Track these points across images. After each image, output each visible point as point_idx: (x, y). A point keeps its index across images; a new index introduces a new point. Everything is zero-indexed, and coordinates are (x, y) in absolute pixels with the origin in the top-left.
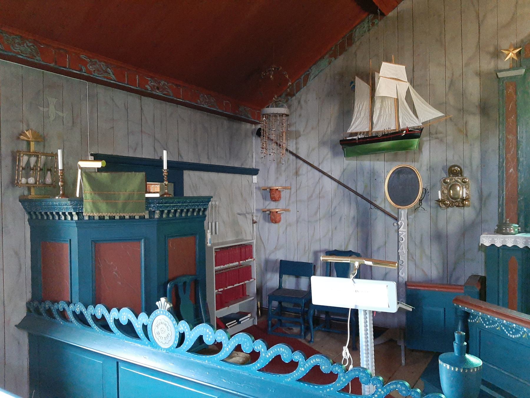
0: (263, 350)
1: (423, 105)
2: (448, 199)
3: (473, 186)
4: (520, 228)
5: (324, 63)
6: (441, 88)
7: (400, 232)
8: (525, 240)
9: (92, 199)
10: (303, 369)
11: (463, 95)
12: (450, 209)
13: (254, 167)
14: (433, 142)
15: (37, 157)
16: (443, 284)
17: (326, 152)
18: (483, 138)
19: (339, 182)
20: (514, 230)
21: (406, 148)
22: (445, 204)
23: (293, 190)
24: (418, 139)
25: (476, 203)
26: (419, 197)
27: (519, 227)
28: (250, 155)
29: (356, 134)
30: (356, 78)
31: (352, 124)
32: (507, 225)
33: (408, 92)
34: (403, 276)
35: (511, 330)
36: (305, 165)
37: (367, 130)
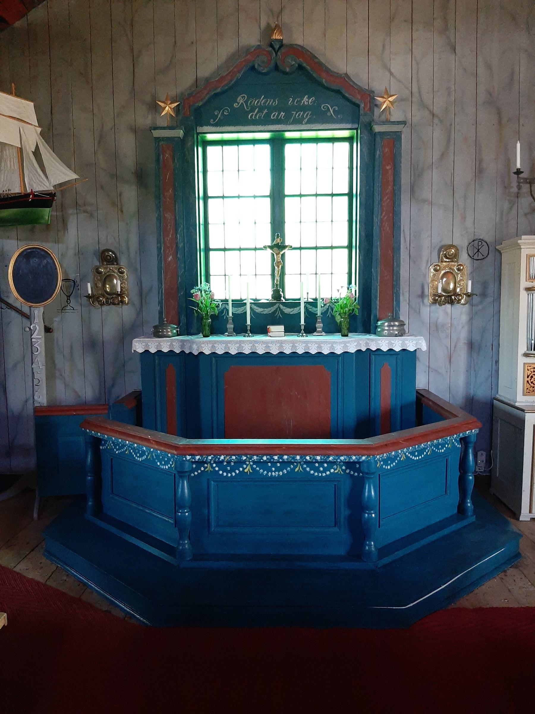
1: (54, 161)
4: (179, 330)
7: (33, 340)
8: (180, 344)
12: (105, 308)
14: (82, 216)
16: (100, 405)
20: (171, 331)
24: (49, 209)
25: (136, 301)
27: (177, 328)
34: (40, 400)
35: (139, 452)
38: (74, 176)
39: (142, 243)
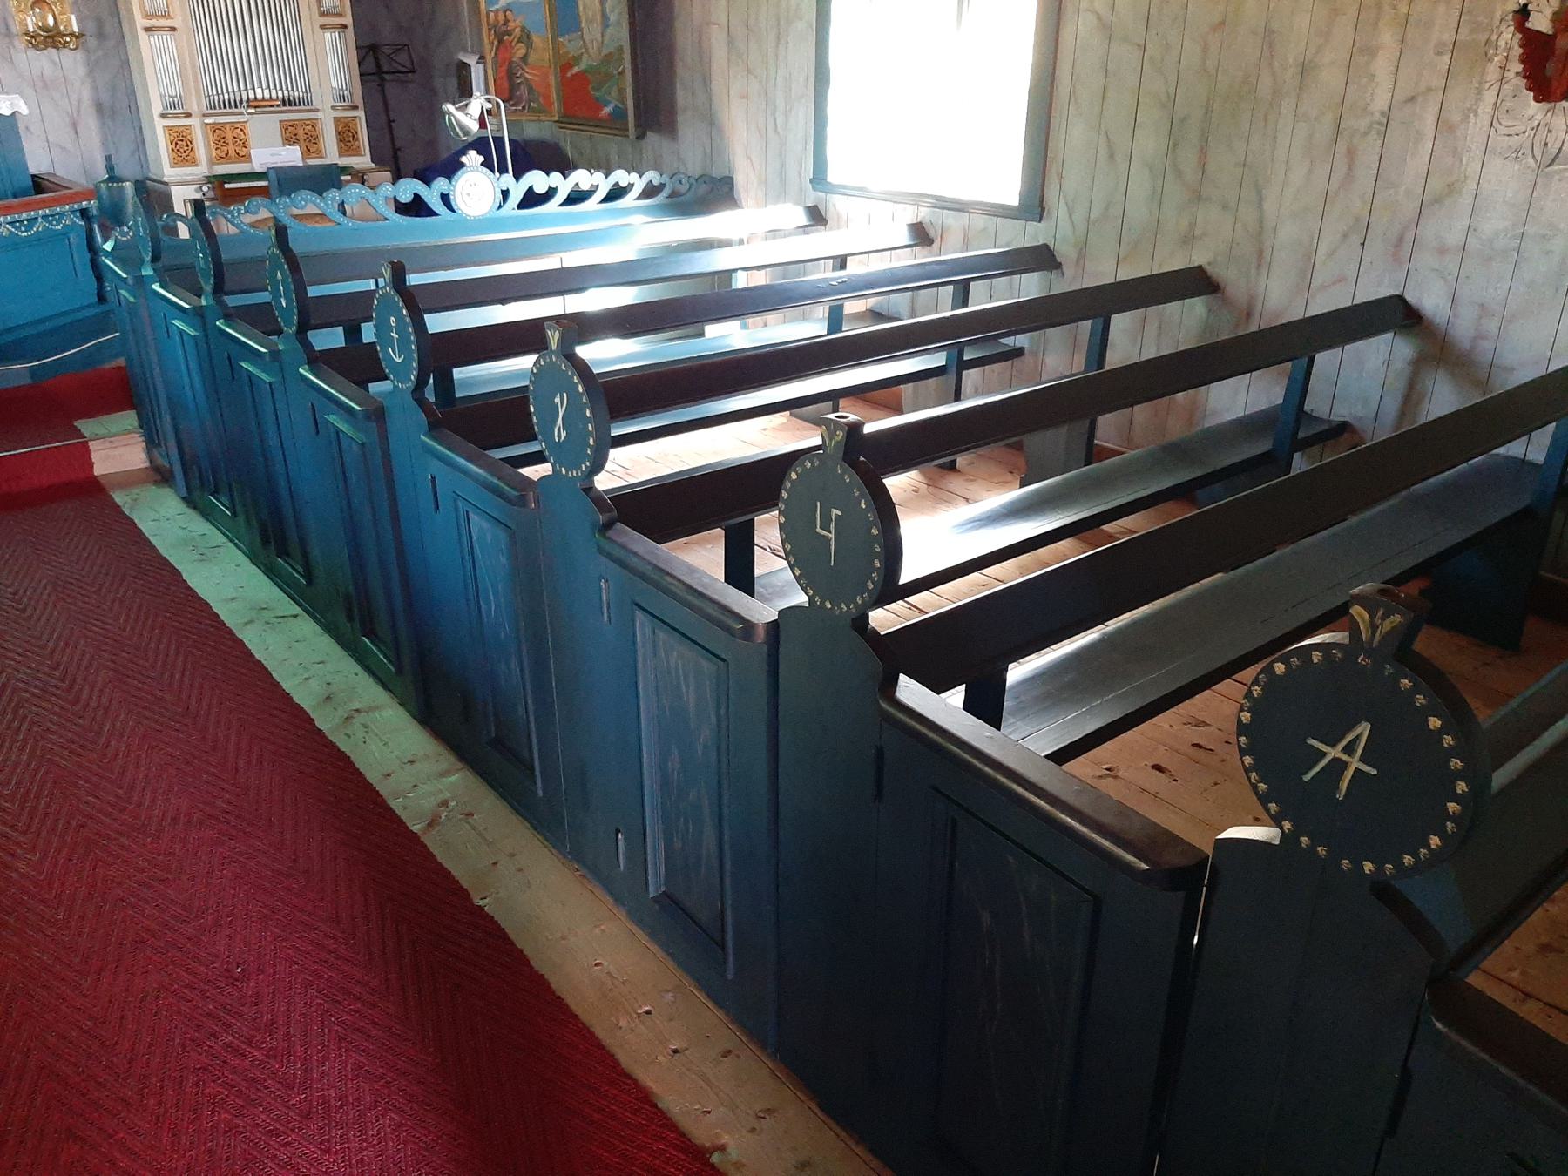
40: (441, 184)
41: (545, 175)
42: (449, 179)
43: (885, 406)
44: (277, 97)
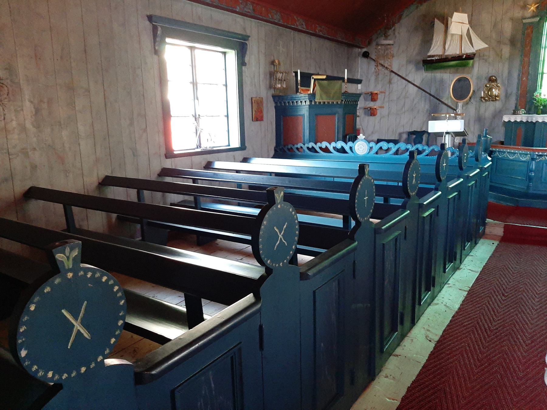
0: (410, 147)
2: (487, 96)
3: (502, 89)
5: (413, 7)
6: (488, 27)
9: (320, 94)
10: (427, 151)
11: (501, 33)
12: (488, 103)
13: (359, 79)
15: (283, 74)
17: (411, 67)
18: (511, 59)
19: (419, 88)
21: (465, 66)
22: (485, 100)
23: (387, 93)
26: (470, 95)
28: (357, 70)
29: (433, 56)
30: (436, 20)
31: (431, 50)
32: (518, 110)
33: (469, 29)
36: (397, 76)
37: (441, 54)
38: (487, 46)
39: (510, 73)
40: (350, 144)
41: (352, 143)
42: (353, 142)
43: (511, 160)
44: (277, 90)
